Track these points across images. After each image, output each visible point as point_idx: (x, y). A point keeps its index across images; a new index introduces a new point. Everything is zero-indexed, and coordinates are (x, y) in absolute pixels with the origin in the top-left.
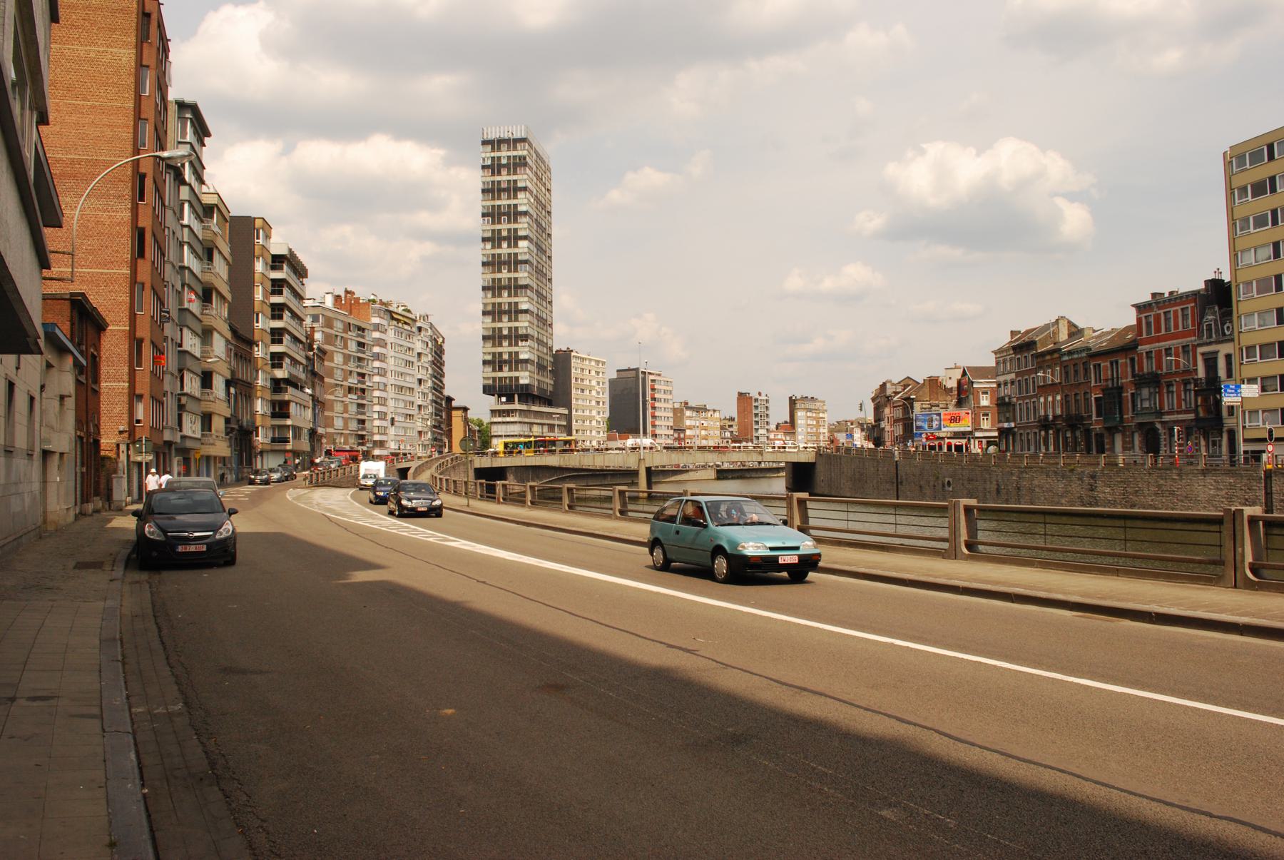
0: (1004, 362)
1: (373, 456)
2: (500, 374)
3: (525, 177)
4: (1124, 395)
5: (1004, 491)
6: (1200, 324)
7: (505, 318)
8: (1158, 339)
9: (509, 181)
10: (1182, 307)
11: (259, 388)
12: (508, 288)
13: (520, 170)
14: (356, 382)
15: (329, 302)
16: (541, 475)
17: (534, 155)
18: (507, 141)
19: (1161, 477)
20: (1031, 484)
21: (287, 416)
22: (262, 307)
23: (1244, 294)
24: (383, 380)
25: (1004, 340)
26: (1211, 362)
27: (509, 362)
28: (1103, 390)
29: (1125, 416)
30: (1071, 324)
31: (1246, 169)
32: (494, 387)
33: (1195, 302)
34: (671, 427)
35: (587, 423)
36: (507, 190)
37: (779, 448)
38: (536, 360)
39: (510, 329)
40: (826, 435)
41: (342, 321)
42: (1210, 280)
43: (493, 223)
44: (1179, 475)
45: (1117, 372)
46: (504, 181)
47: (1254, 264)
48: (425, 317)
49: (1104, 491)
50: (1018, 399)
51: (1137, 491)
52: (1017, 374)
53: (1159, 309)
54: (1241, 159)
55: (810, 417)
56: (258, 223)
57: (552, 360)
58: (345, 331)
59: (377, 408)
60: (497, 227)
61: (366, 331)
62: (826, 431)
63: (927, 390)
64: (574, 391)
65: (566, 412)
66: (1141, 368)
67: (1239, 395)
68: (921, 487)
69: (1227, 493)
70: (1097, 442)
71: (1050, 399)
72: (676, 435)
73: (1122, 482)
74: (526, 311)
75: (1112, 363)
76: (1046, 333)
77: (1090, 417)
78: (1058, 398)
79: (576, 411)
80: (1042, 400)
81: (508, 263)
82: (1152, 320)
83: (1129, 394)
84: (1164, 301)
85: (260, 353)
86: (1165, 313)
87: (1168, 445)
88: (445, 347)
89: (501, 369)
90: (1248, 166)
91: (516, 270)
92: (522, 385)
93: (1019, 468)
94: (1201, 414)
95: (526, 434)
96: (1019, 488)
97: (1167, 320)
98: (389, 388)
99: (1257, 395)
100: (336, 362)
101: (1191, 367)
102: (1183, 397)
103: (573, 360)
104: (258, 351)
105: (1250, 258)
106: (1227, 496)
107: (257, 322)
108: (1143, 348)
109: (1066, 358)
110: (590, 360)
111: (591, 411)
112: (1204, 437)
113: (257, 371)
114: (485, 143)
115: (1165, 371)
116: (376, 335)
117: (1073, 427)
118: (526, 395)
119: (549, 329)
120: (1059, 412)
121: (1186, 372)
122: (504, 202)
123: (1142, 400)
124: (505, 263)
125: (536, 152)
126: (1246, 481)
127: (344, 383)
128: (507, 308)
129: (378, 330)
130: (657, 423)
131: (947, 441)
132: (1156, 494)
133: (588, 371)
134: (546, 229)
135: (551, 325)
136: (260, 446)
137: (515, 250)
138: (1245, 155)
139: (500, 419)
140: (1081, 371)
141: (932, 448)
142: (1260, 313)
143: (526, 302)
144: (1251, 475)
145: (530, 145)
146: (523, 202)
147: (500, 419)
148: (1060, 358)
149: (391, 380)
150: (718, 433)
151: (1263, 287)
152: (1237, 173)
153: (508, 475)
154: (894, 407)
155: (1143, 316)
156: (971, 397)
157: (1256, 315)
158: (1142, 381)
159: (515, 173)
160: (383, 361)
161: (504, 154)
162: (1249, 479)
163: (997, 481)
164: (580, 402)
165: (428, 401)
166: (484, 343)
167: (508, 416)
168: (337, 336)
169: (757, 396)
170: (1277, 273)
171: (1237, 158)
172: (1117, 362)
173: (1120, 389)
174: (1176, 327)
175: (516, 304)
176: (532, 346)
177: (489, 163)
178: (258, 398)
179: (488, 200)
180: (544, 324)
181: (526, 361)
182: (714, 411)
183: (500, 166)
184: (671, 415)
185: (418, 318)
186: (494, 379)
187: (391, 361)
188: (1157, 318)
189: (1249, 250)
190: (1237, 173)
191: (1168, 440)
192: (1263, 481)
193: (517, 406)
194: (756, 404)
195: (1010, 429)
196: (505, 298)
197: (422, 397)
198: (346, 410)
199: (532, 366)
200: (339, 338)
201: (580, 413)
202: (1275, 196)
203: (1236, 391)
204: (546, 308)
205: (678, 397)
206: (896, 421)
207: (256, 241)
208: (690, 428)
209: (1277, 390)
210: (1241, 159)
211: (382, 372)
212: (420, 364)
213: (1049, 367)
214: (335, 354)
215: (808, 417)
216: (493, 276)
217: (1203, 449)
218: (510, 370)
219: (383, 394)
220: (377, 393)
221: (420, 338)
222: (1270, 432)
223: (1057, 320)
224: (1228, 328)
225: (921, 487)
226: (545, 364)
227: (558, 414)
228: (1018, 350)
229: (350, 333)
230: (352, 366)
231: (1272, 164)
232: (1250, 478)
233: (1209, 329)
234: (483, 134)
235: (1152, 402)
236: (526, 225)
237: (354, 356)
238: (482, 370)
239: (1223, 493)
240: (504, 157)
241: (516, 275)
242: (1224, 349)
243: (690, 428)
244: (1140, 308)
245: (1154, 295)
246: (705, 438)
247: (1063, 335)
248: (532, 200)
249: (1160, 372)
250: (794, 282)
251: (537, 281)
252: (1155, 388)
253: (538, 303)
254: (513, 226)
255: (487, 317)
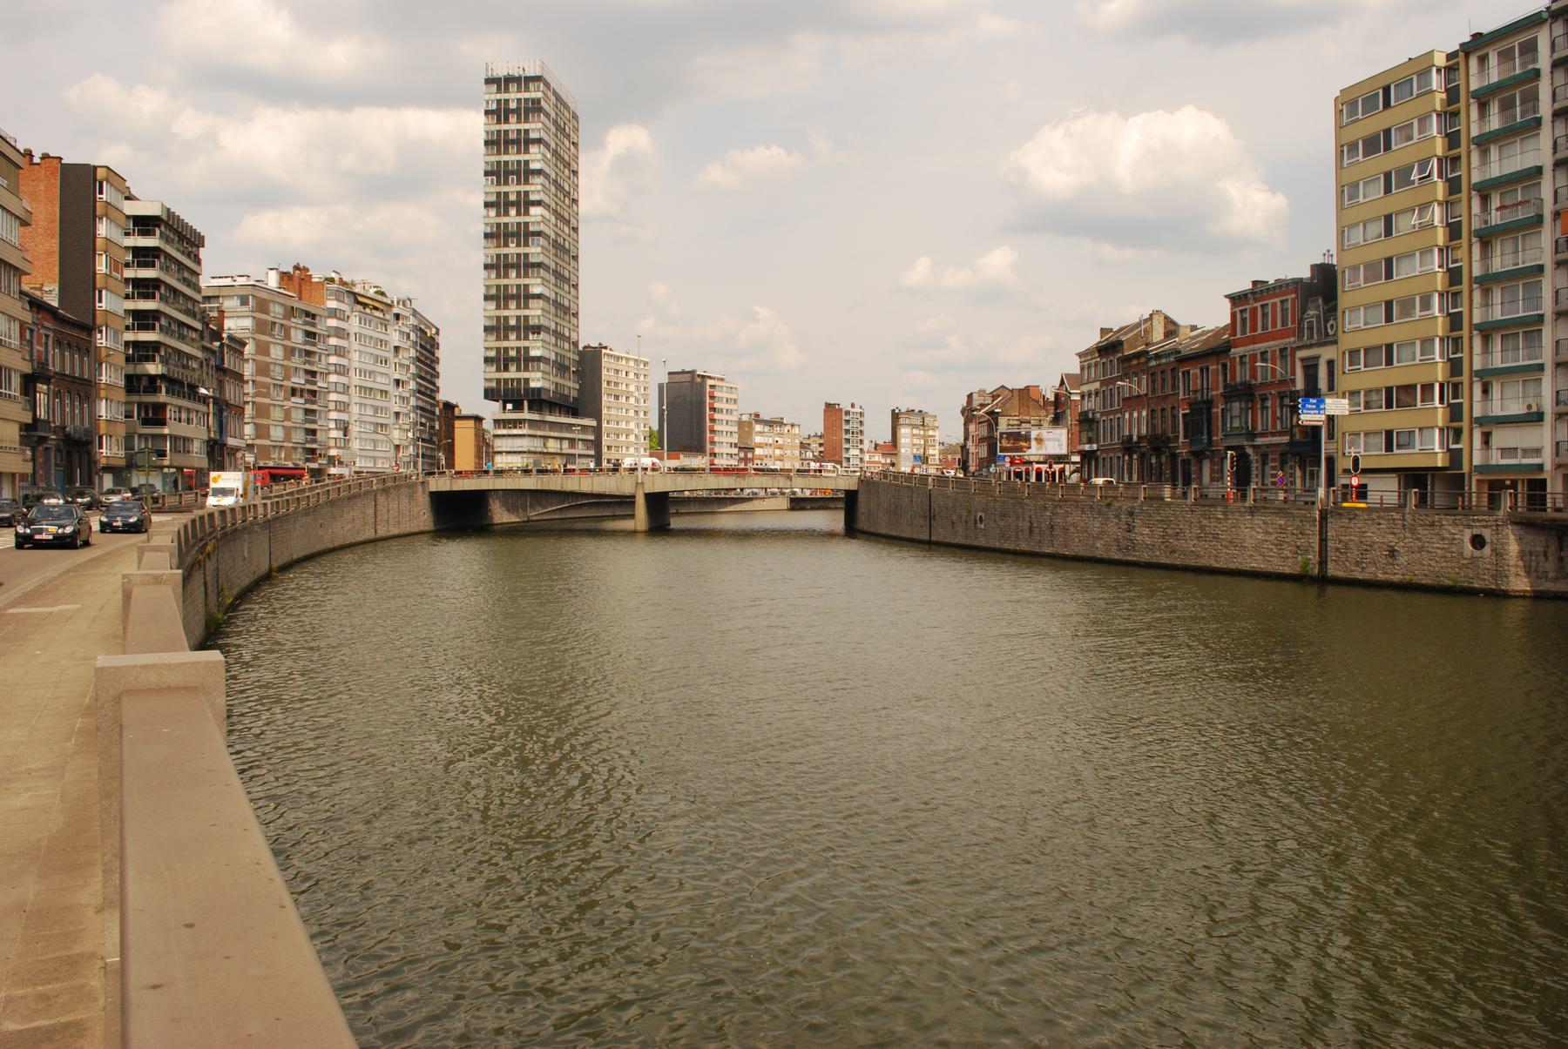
0: (1089, 367)
1: (329, 475)
2: (505, 375)
3: (539, 125)
4: (1214, 410)
5: (1037, 530)
6: (1301, 321)
7: (513, 305)
8: (1254, 340)
9: (519, 131)
10: (1282, 298)
11: (102, 386)
12: (517, 266)
13: (533, 116)
14: (303, 382)
15: (273, 281)
16: (544, 502)
17: (553, 99)
18: (517, 80)
19: (1204, 515)
20: (1066, 522)
21: (163, 423)
22: (106, 282)
23: (1350, 282)
24: (343, 380)
25: (1094, 339)
26: (1311, 368)
27: (517, 360)
28: (1190, 404)
29: (1215, 438)
30: (1168, 321)
31: (1358, 120)
32: (499, 391)
33: (1296, 292)
34: (736, 444)
35: (623, 438)
36: (517, 142)
37: (815, 471)
38: (553, 357)
39: (518, 318)
40: (937, 457)
41: (283, 305)
42: (1317, 265)
43: (499, 183)
44: (1225, 513)
45: (1208, 381)
46: (513, 131)
47: (1362, 243)
48: (404, 302)
49: (1143, 534)
50: (1102, 414)
51: (1178, 533)
52: (1103, 383)
53: (1256, 300)
54: (1352, 104)
55: (916, 435)
56: (101, 174)
57: (577, 358)
58: (286, 317)
59: (333, 415)
60: (504, 189)
61: (318, 318)
62: (936, 452)
63: (1016, 401)
64: (605, 398)
65: (594, 423)
66: (1233, 377)
67: (1322, 412)
68: (953, 523)
69: (1276, 538)
70: (1183, 470)
71: (1135, 415)
72: (742, 455)
73: (1162, 521)
74: (539, 296)
75: (1202, 370)
76: (1136, 331)
77: (1177, 437)
78: (1144, 413)
79: (608, 423)
80: (1127, 416)
81: (517, 235)
82: (1247, 315)
83: (1220, 410)
84: (1268, 290)
85: (104, 341)
86: (1262, 306)
87: (1260, 477)
88: (440, 340)
89: (506, 369)
90: (1360, 116)
91: (526, 245)
92: (534, 389)
93: (1054, 500)
94: (1298, 437)
95: (539, 450)
96: (1052, 527)
97: (1264, 315)
98: (352, 390)
99: (1347, 413)
100: (273, 356)
101: (1289, 376)
102: (1278, 415)
103: (605, 360)
104: (101, 339)
105: (1357, 236)
106: (1276, 542)
107: (100, 301)
108: (1236, 352)
109: (1153, 363)
110: (628, 359)
111: (627, 423)
112: (1300, 466)
113: (101, 364)
114: (489, 81)
115: (1259, 380)
116: (332, 323)
117: (1157, 451)
118: (538, 401)
119: (574, 320)
120: (1144, 431)
121: (1283, 382)
122: (512, 157)
123: (1231, 418)
124: (512, 235)
125: (555, 94)
126: (1298, 523)
127: (285, 383)
128: (515, 292)
129: (335, 317)
130: (716, 439)
131: (1036, 466)
132: (1198, 537)
133: (624, 373)
134: (569, 193)
135: (576, 315)
136: (104, 461)
137: (527, 219)
138: (1357, 101)
139: (504, 432)
140: (1169, 381)
141: (1018, 475)
142: (1367, 307)
143: (538, 285)
144: (1304, 516)
145: (547, 85)
146: (536, 157)
147: (504, 432)
148: (1147, 362)
149: (355, 380)
150: (797, 453)
151: (1371, 271)
152: (1347, 125)
153: (491, 501)
154: (980, 423)
155: (1238, 310)
156: (1068, 412)
157: (1362, 309)
158: (1232, 393)
159: (527, 121)
160: (343, 356)
161: (513, 96)
162: (1301, 521)
163: (1030, 517)
164: (613, 412)
165: (409, 408)
166: (486, 336)
167: (515, 427)
168: (275, 323)
169: (849, 408)
170: (1387, 256)
171: (1353, 103)
172: (1207, 369)
173: (1209, 403)
174: (1274, 324)
175: (526, 286)
176: (548, 340)
177: (494, 107)
178: (101, 400)
179: (492, 155)
180: (565, 313)
181: (539, 359)
182: (793, 425)
183: (508, 111)
184: (735, 429)
185: (395, 303)
186: (498, 381)
187: (355, 356)
188: (1254, 312)
189: (1357, 225)
190: (1347, 125)
191: (1260, 468)
192: (1317, 524)
193: (526, 415)
194: (847, 418)
195: (1092, 452)
196: (513, 280)
197: (403, 402)
198: (287, 416)
199: (547, 366)
200: (277, 326)
201: (612, 425)
202: (1390, 155)
203: (1318, 406)
204: (569, 293)
205: (745, 409)
206: (982, 440)
207: (98, 196)
208: (760, 446)
209: (1381, 407)
210: (1352, 104)
211: (342, 371)
212: (397, 360)
213: (1136, 374)
214: (272, 346)
215: (914, 435)
216: (498, 251)
217: (1298, 481)
218: (518, 369)
219: (344, 398)
220: (333, 397)
221: (397, 328)
222: (1356, 460)
223: (1151, 315)
224: (1332, 326)
225: (953, 523)
226: (567, 363)
227: (579, 425)
228: (1103, 353)
229: (293, 320)
230: (297, 361)
231: (1389, 112)
232: (1304, 519)
233: (1311, 328)
234: (487, 70)
235: (1243, 421)
236: (539, 188)
237: (300, 350)
238: (483, 369)
239: (1273, 537)
240: (513, 100)
241: (527, 250)
242: (1327, 353)
243: (760, 446)
244: (1236, 299)
245: (1255, 283)
246: (780, 459)
247: (1158, 334)
248: (549, 156)
249: (1254, 382)
250: (920, 271)
251: (555, 258)
252: (1247, 403)
253: (556, 286)
254: (523, 188)
255: (489, 302)
